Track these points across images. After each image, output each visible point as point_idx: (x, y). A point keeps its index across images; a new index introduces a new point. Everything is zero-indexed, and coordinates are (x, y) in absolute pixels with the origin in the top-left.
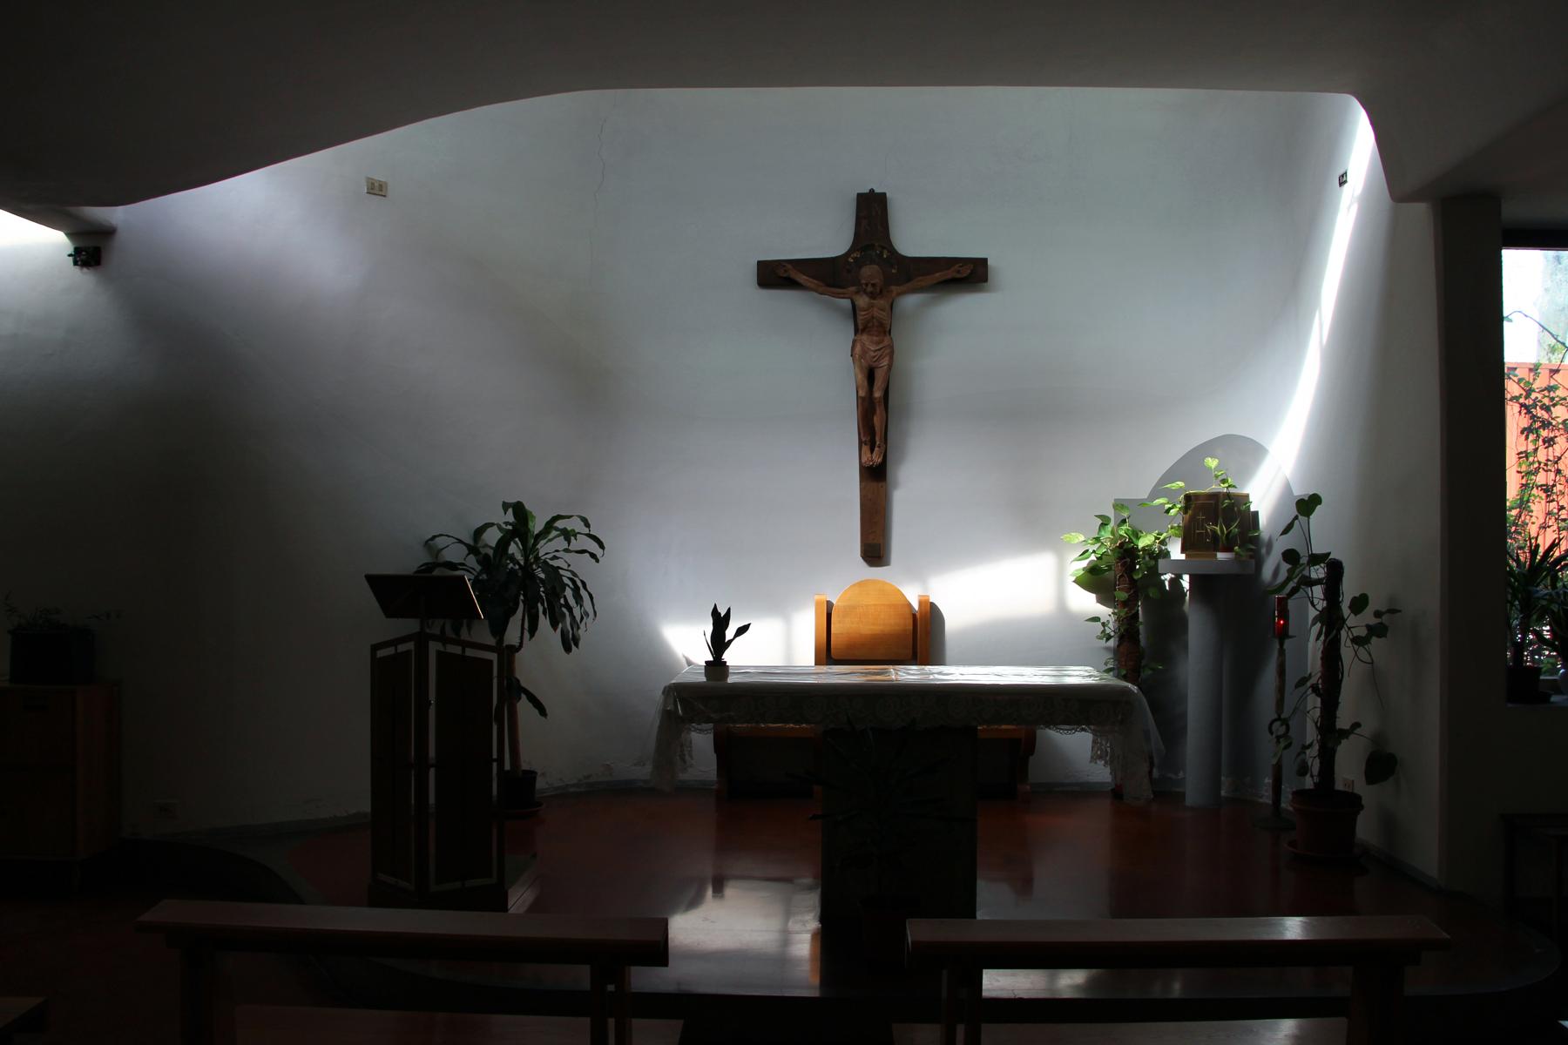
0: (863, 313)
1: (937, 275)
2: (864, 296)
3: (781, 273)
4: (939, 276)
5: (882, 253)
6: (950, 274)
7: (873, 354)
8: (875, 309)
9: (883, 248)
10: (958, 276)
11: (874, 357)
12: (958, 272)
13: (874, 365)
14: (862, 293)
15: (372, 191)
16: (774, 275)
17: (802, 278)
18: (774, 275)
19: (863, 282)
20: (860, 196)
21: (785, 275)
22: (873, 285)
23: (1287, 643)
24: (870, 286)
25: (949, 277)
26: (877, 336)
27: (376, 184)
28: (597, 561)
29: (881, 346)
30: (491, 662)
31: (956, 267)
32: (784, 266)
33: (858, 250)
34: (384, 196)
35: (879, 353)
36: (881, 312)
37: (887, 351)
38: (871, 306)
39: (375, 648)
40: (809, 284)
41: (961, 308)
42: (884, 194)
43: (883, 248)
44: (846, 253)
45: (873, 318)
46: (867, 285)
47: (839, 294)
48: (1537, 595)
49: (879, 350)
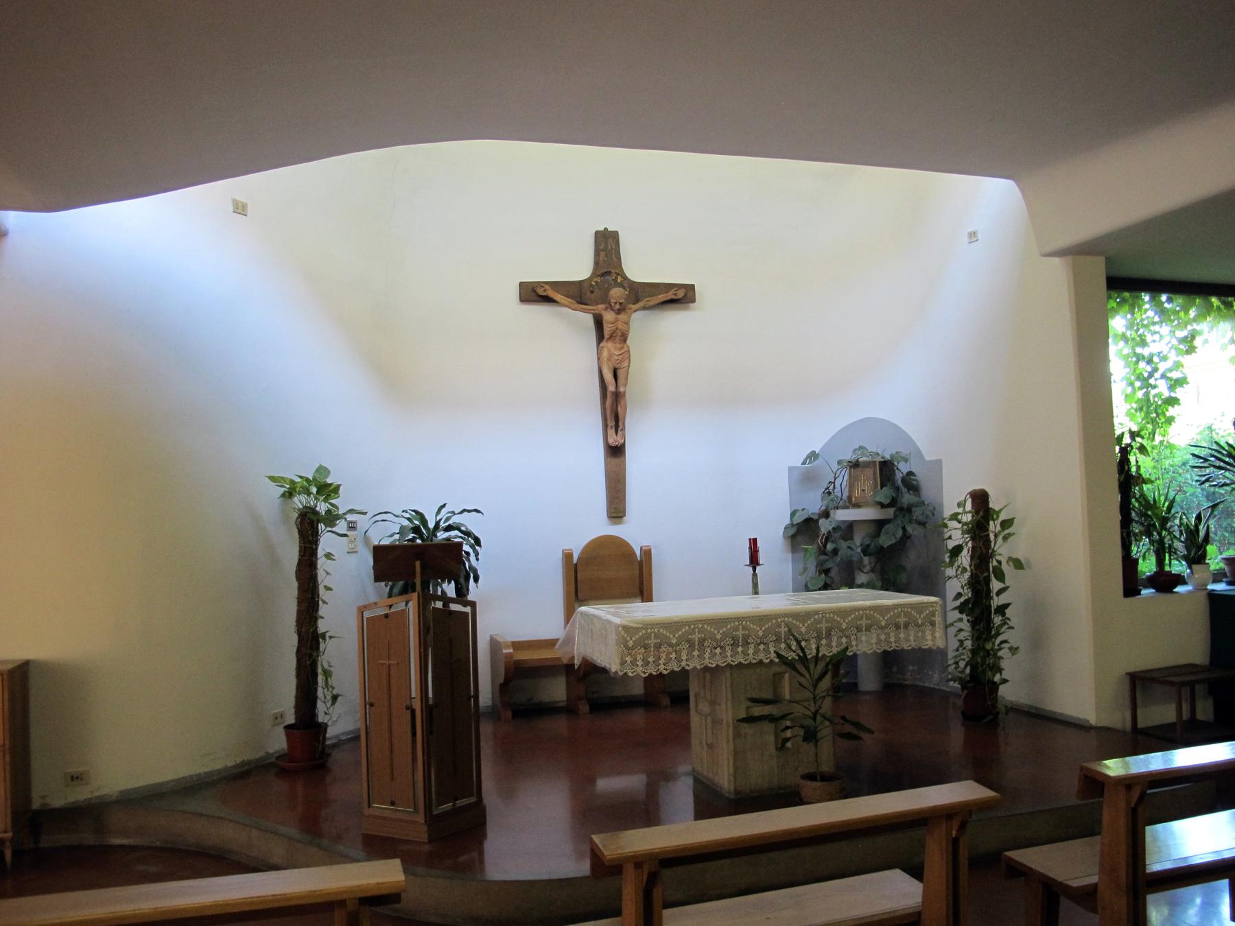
0: (609, 326)
1: (661, 296)
2: (612, 312)
3: (541, 292)
4: (662, 297)
5: (616, 278)
6: (670, 296)
7: (617, 358)
8: (620, 322)
9: (618, 274)
10: (676, 298)
11: (618, 360)
12: (676, 295)
13: (617, 366)
14: (609, 310)
15: (236, 210)
16: (534, 294)
17: (558, 297)
18: (534, 294)
19: (612, 300)
20: (597, 232)
21: (544, 294)
22: (620, 304)
23: (758, 568)
24: (618, 304)
25: (668, 299)
26: (619, 343)
27: (240, 205)
28: (753, 542)
29: (622, 351)
30: (468, 613)
31: (673, 291)
32: (543, 287)
33: (599, 276)
34: (246, 215)
35: (621, 357)
36: (624, 325)
37: (627, 356)
38: (617, 320)
39: (361, 611)
40: (563, 302)
41: (673, 320)
42: (617, 232)
43: (618, 274)
44: (590, 277)
45: (617, 328)
46: (616, 303)
47: (587, 310)
48: (1183, 545)
49: (620, 355)
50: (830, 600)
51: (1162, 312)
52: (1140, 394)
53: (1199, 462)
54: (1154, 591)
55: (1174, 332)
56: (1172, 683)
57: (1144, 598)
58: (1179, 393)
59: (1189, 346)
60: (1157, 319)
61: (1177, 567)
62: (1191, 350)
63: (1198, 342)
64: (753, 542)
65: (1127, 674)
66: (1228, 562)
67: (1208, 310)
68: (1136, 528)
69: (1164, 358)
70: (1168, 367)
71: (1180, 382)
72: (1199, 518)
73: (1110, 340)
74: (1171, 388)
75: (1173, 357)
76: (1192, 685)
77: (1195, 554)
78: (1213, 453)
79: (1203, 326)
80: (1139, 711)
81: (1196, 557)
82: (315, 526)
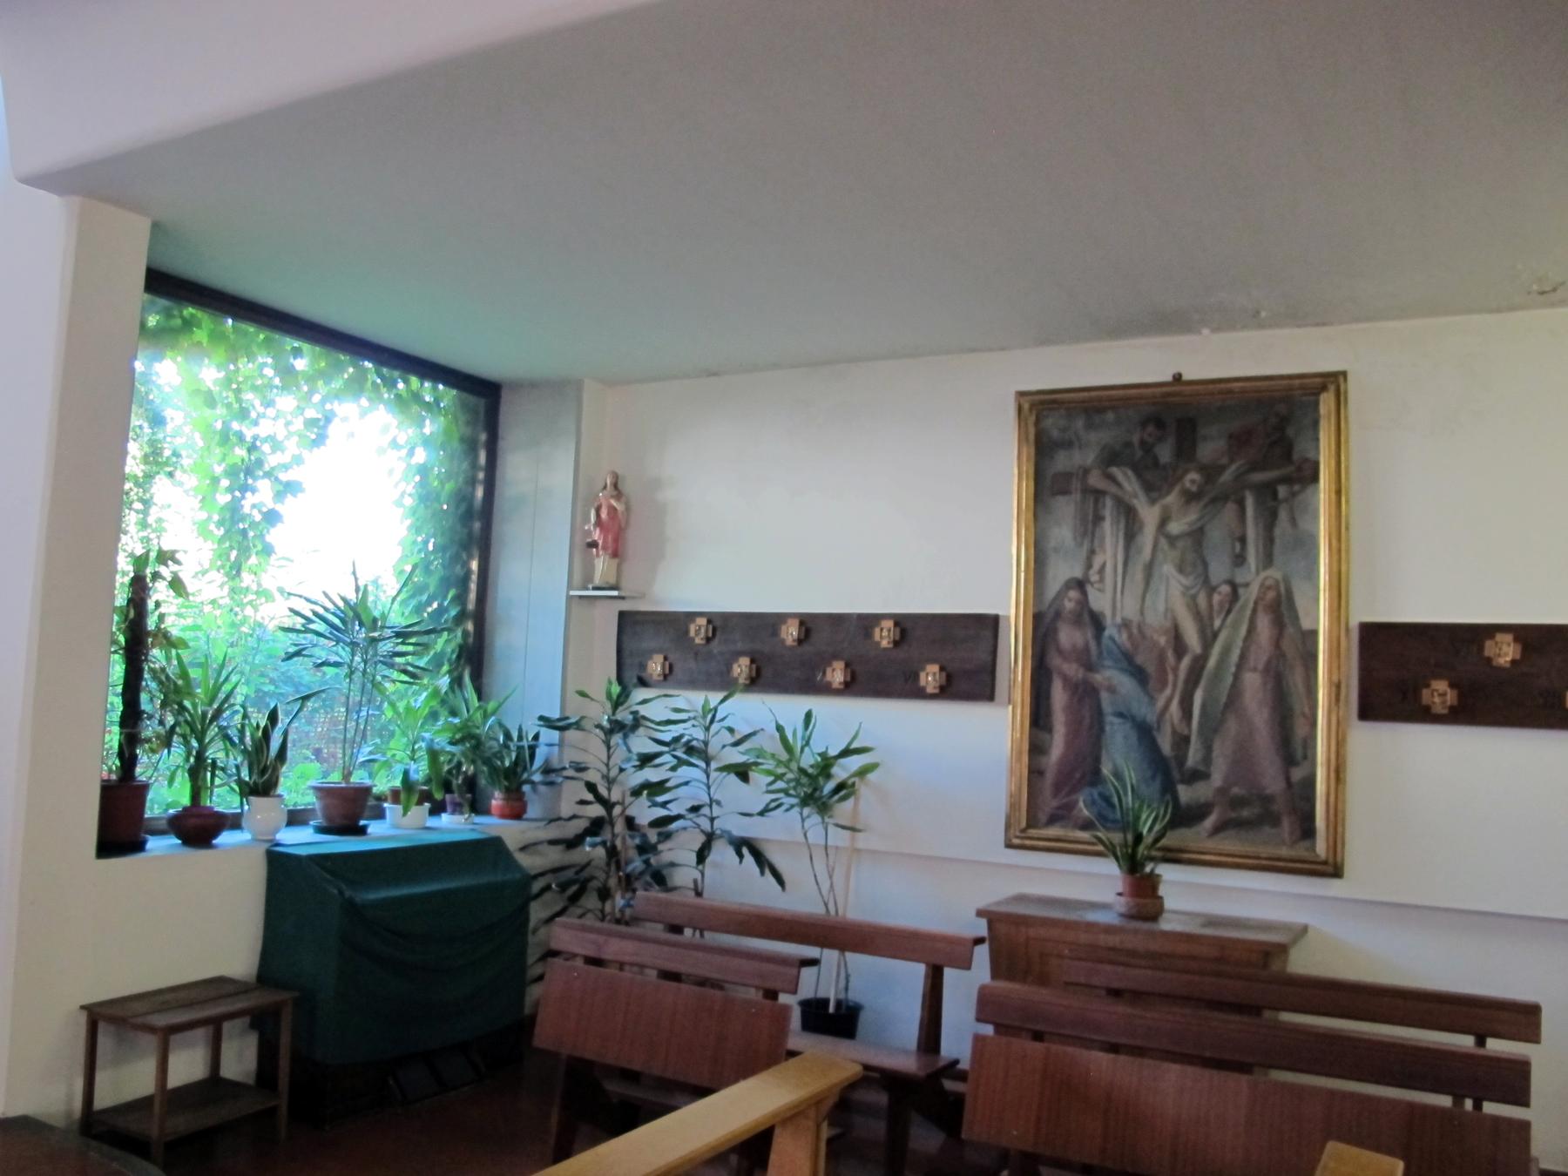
28: (292, 561)
50: (1324, 447)
51: (287, 373)
52: (224, 498)
53: (298, 622)
54: (180, 842)
55: (304, 409)
56: (152, 1029)
57: (157, 858)
58: (287, 508)
59: (318, 430)
60: (277, 381)
61: (223, 798)
62: (320, 440)
63: (333, 429)
64: (292, 561)
65: (83, 1007)
66: (319, 794)
67: (356, 386)
68: (149, 729)
69: (277, 446)
70: (282, 462)
71: (288, 489)
72: (273, 717)
73: (133, 415)
74: (279, 496)
75: (292, 447)
76: (216, 1024)
77: (413, 735)
78: (321, 611)
79: (347, 409)
80: (100, 1077)
81: (262, 785)
82: (1318, 380)
